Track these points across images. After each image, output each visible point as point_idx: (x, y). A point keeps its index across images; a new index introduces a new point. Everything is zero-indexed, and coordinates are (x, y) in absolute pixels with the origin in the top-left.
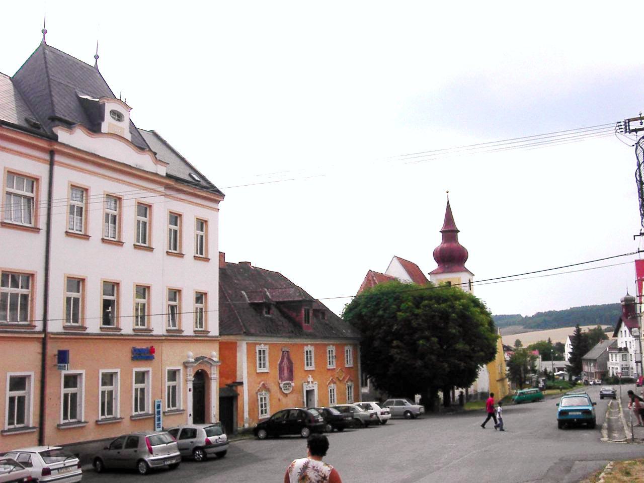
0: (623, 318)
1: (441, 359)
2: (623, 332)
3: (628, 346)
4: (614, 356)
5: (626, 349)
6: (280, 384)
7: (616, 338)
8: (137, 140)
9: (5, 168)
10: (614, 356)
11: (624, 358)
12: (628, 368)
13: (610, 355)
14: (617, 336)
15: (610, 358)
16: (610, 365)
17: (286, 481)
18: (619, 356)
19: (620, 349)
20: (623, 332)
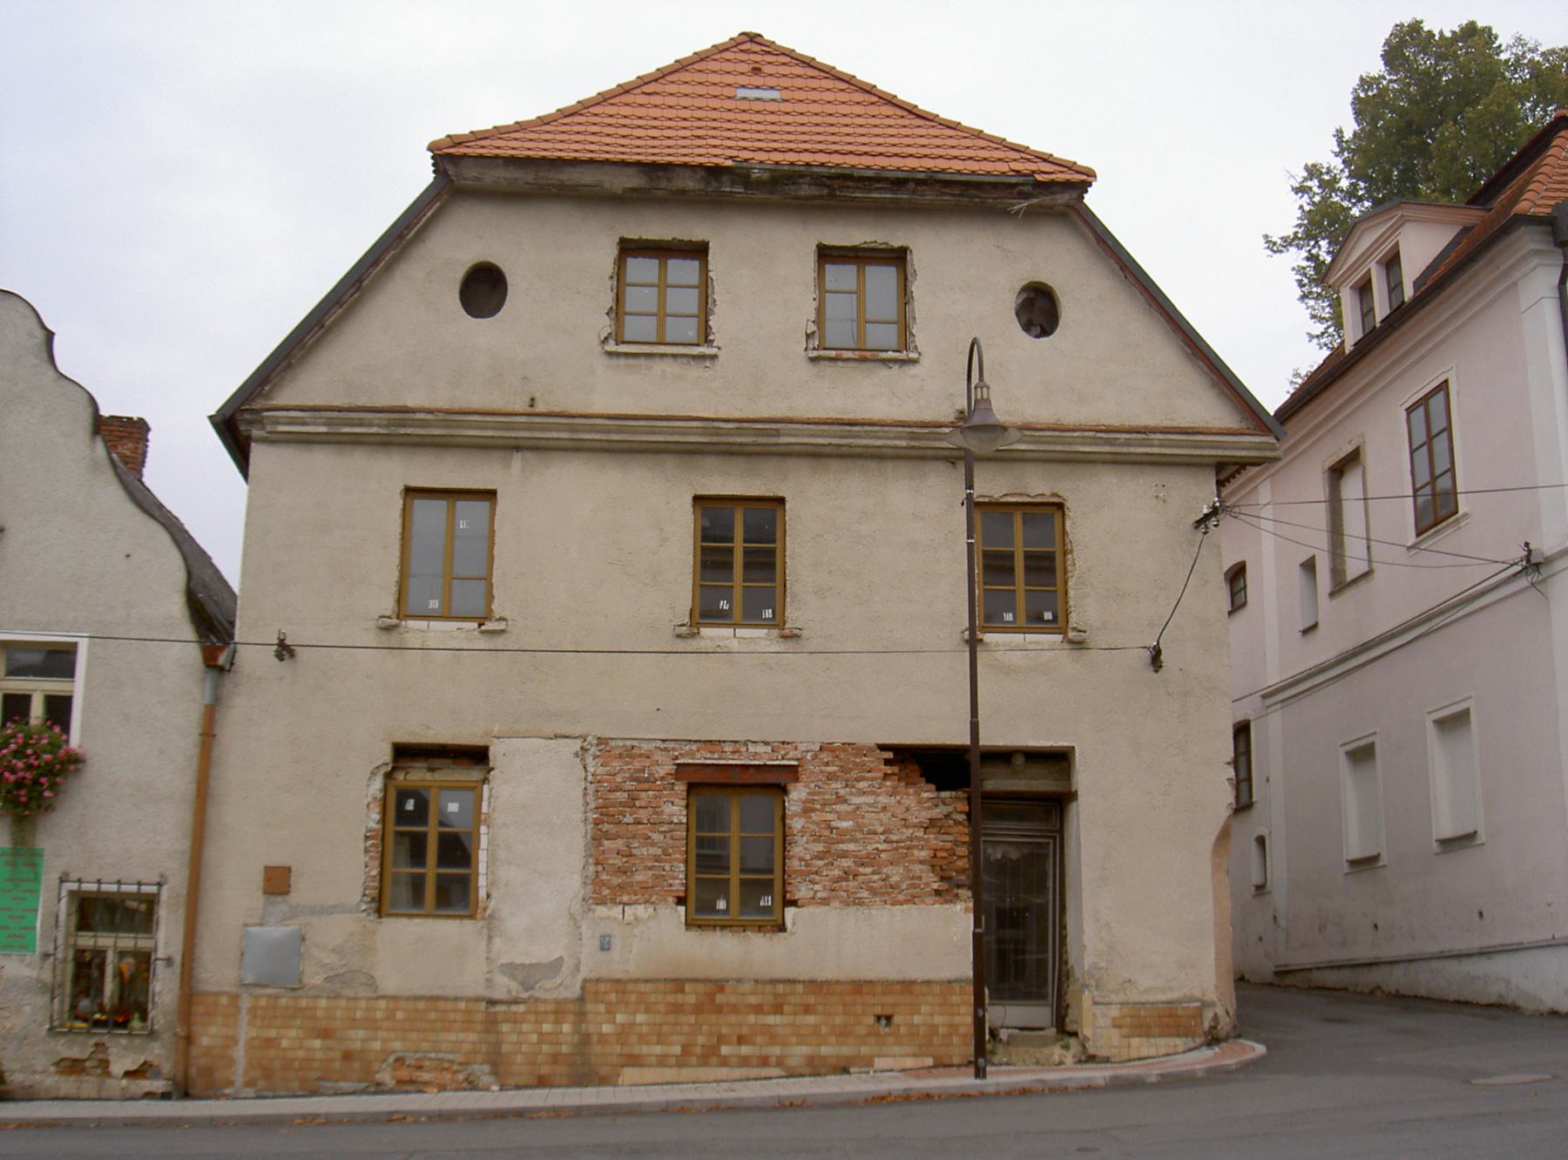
1: (625, 898)
8: (629, 819)
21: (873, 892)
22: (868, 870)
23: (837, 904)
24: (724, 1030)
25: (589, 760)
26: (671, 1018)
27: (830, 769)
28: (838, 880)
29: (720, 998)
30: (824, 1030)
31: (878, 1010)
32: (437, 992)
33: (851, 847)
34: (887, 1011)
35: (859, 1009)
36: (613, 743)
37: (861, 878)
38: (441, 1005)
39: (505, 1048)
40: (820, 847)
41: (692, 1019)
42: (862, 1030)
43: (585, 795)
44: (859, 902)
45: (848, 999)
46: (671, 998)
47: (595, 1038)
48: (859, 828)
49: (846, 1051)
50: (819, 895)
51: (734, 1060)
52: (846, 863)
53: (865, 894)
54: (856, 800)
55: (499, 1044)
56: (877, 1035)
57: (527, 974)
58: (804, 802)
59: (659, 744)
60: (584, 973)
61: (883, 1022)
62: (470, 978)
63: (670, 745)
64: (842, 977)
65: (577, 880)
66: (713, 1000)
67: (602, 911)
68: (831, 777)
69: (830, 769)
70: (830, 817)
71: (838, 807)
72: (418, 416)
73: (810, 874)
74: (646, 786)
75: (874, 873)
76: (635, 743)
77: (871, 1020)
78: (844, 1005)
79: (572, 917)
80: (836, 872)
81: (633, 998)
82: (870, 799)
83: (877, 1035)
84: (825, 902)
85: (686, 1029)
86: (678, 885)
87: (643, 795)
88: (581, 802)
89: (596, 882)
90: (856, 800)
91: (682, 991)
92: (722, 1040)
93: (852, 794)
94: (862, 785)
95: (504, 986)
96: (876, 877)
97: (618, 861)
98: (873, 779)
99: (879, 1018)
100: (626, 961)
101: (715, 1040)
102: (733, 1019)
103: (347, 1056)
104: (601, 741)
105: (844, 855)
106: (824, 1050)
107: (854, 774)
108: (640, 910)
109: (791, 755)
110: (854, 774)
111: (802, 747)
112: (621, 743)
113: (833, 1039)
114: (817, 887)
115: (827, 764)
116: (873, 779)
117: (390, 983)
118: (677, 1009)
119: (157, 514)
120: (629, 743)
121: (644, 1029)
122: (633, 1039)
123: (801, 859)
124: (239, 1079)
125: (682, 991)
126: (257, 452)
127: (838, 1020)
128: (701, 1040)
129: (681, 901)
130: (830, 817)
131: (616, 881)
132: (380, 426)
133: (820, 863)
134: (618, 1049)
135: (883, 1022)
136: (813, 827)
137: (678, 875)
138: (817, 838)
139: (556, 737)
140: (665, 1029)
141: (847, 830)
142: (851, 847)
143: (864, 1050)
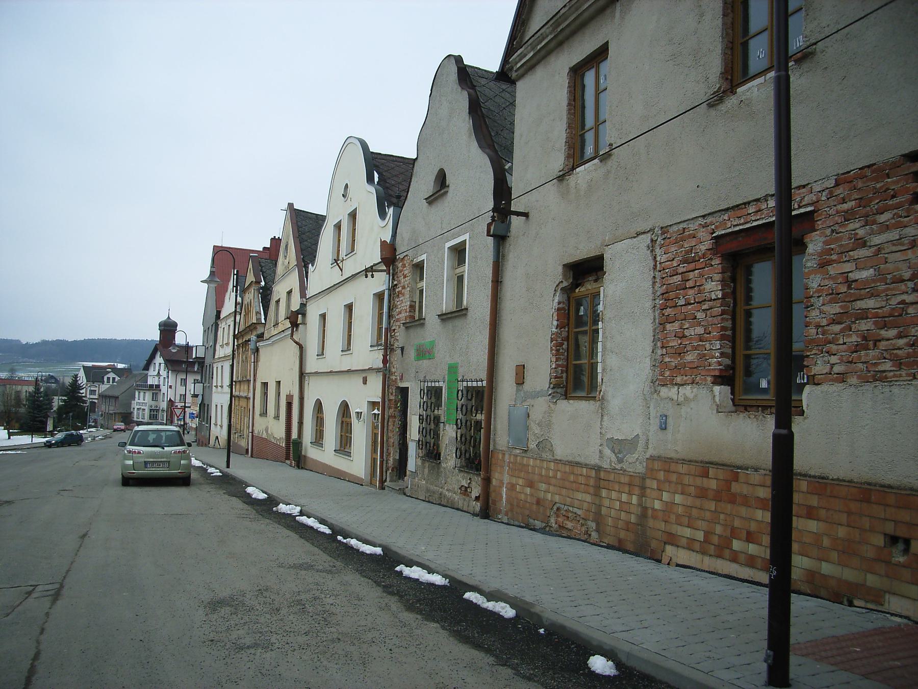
0: (160, 347)
1: (679, 379)
2: (157, 365)
3: (161, 383)
4: (142, 394)
5: (158, 386)
6: (196, 429)
7: (146, 372)
8: (682, 302)
9: (291, 205)
10: (142, 394)
11: (155, 397)
12: (157, 411)
13: (137, 393)
14: (148, 370)
15: (137, 396)
16: (135, 405)
17: (771, 682)
18: (149, 395)
19: (151, 386)
20: (157, 365)
21: (899, 363)
22: (892, 333)
23: (854, 380)
24: (737, 523)
25: (658, 251)
26: (698, 502)
27: (845, 206)
28: (857, 348)
29: (735, 487)
30: (826, 542)
31: (890, 528)
32: (578, 459)
33: (870, 303)
34: (902, 532)
35: (866, 523)
36: (671, 230)
37: (883, 345)
38: (578, 470)
39: (604, 511)
40: (836, 309)
41: (712, 505)
42: (870, 553)
43: (654, 283)
44: (879, 377)
45: (854, 506)
46: (699, 481)
47: (650, 512)
48: (881, 276)
49: (849, 575)
50: (837, 369)
51: (742, 558)
52: (865, 326)
53: (887, 366)
54: (876, 240)
55: (600, 506)
56: (888, 563)
57: (620, 446)
58: (820, 254)
59: (701, 221)
60: (651, 452)
61: (901, 546)
62: (591, 452)
63: (709, 220)
64: (854, 476)
65: (648, 362)
66: (729, 489)
67: (664, 392)
68: (848, 216)
69: (845, 206)
70: (847, 267)
71: (855, 254)
72: (562, 12)
73: (824, 345)
74: (692, 266)
75: (900, 336)
76: (684, 225)
77: (879, 541)
78: (849, 513)
79: (645, 399)
80: (854, 339)
81: (674, 477)
82: (893, 235)
83: (888, 563)
84: (842, 378)
85: (708, 515)
86: (716, 362)
87: (691, 275)
88: (651, 290)
89: (663, 365)
90: (876, 240)
91: (706, 475)
92: (734, 533)
93: (872, 233)
94: (883, 218)
95: (609, 459)
96: (901, 342)
97: (674, 343)
98: (898, 206)
99: (893, 540)
100: (677, 442)
101: (728, 533)
102: (743, 511)
103: (538, 502)
104: (664, 230)
105: (863, 315)
106: (826, 568)
107: (874, 205)
108: (687, 391)
109: (807, 200)
110: (874, 205)
111: (817, 188)
112: (675, 228)
113: (834, 555)
114: (834, 359)
115: (844, 201)
116: (898, 206)
117: (562, 450)
118: (702, 493)
119: (579, 103)
120: (681, 226)
121: (680, 510)
122: (673, 518)
123: (818, 326)
124: (504, 510)
125: (706, 475)
126: (206, 285)
127: (842, 532)
128: (719, 529)
129: (721, 379)
130: (847, 267)
131: (674, 362)
132: (551, 33)
133: (837, 328)
134: (662, 526)
135: (901, 546)
136: (830, 283)
137: (715, 353)
138: (834, 296)
139: (638, 234)
140: (695, 512)
141: (866, 281)
142: (870, 303)
143: (872, 580)
